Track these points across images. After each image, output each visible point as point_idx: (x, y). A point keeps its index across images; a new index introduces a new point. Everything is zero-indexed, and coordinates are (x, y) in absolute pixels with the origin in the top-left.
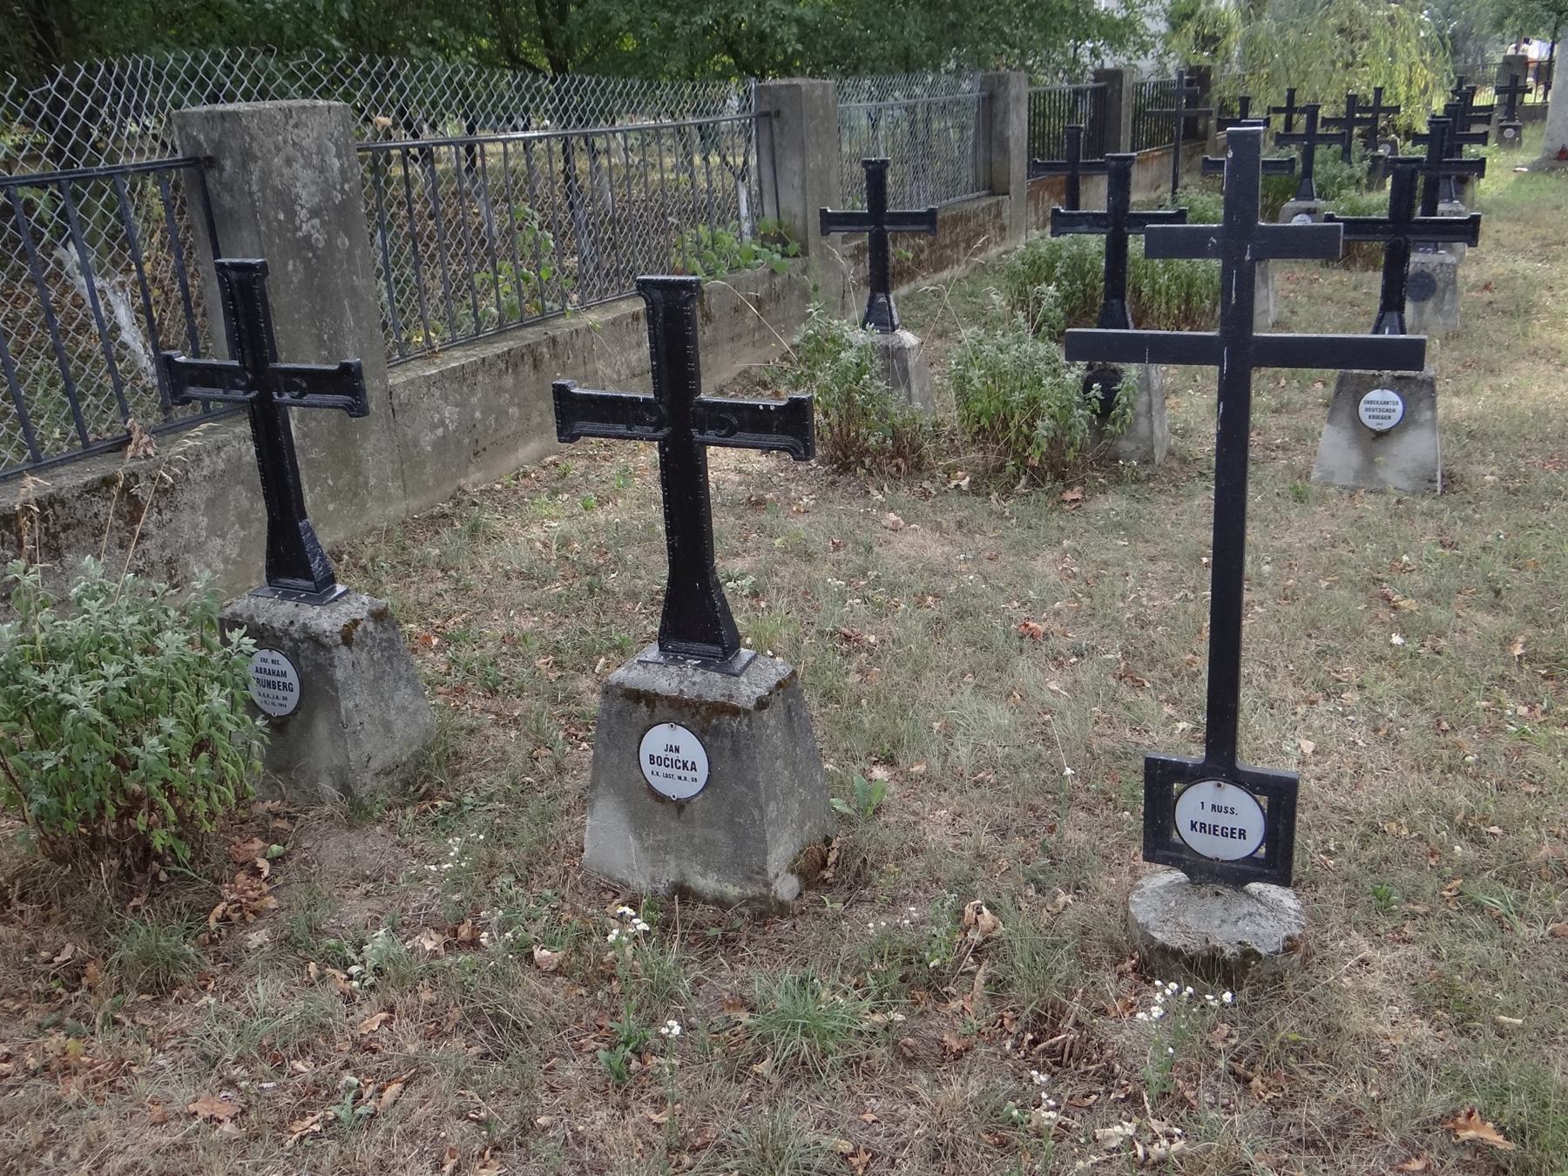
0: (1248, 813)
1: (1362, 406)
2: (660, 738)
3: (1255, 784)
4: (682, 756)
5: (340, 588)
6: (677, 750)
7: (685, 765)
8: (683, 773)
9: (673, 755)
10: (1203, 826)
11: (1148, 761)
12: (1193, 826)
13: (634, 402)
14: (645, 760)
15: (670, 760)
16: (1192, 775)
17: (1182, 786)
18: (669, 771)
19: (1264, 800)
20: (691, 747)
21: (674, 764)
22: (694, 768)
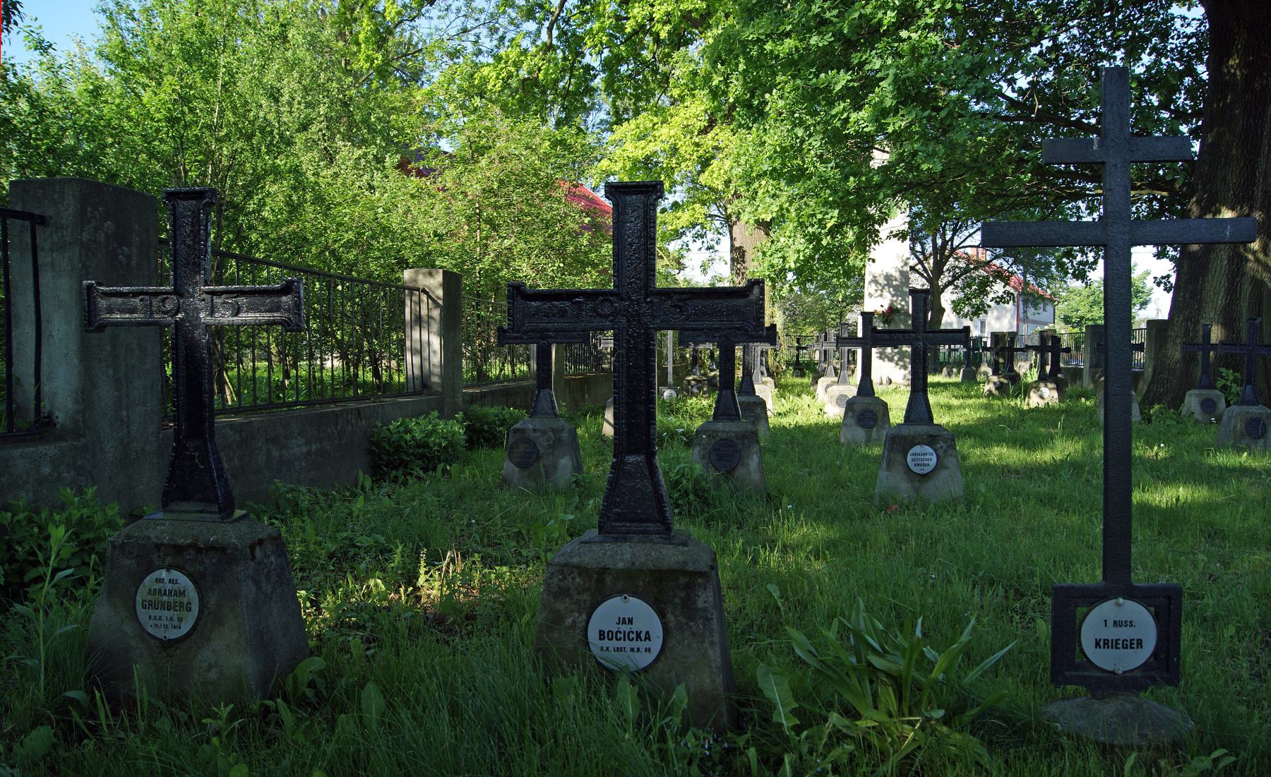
0: (1142, 622)
1: (909, 458)
2: (609, 612)
3: (1142, 596)
4: (636, 627)
5: (238, 513)
6: (631, 621)
7: (638, 635)
8: (635, 644)
9: (624, 628)
10: (1106, 642)
11: (1177, 686)
12: (1097, 644)
13: (1127, 569)
14: (593, 635)
15: (627, 632)
16: (1094, 597)
17: (1085, 609)
18: (621, 644)
19: (1152, 609)
20: (643, 615)
21: (627, 636)
22: (648, 637)
